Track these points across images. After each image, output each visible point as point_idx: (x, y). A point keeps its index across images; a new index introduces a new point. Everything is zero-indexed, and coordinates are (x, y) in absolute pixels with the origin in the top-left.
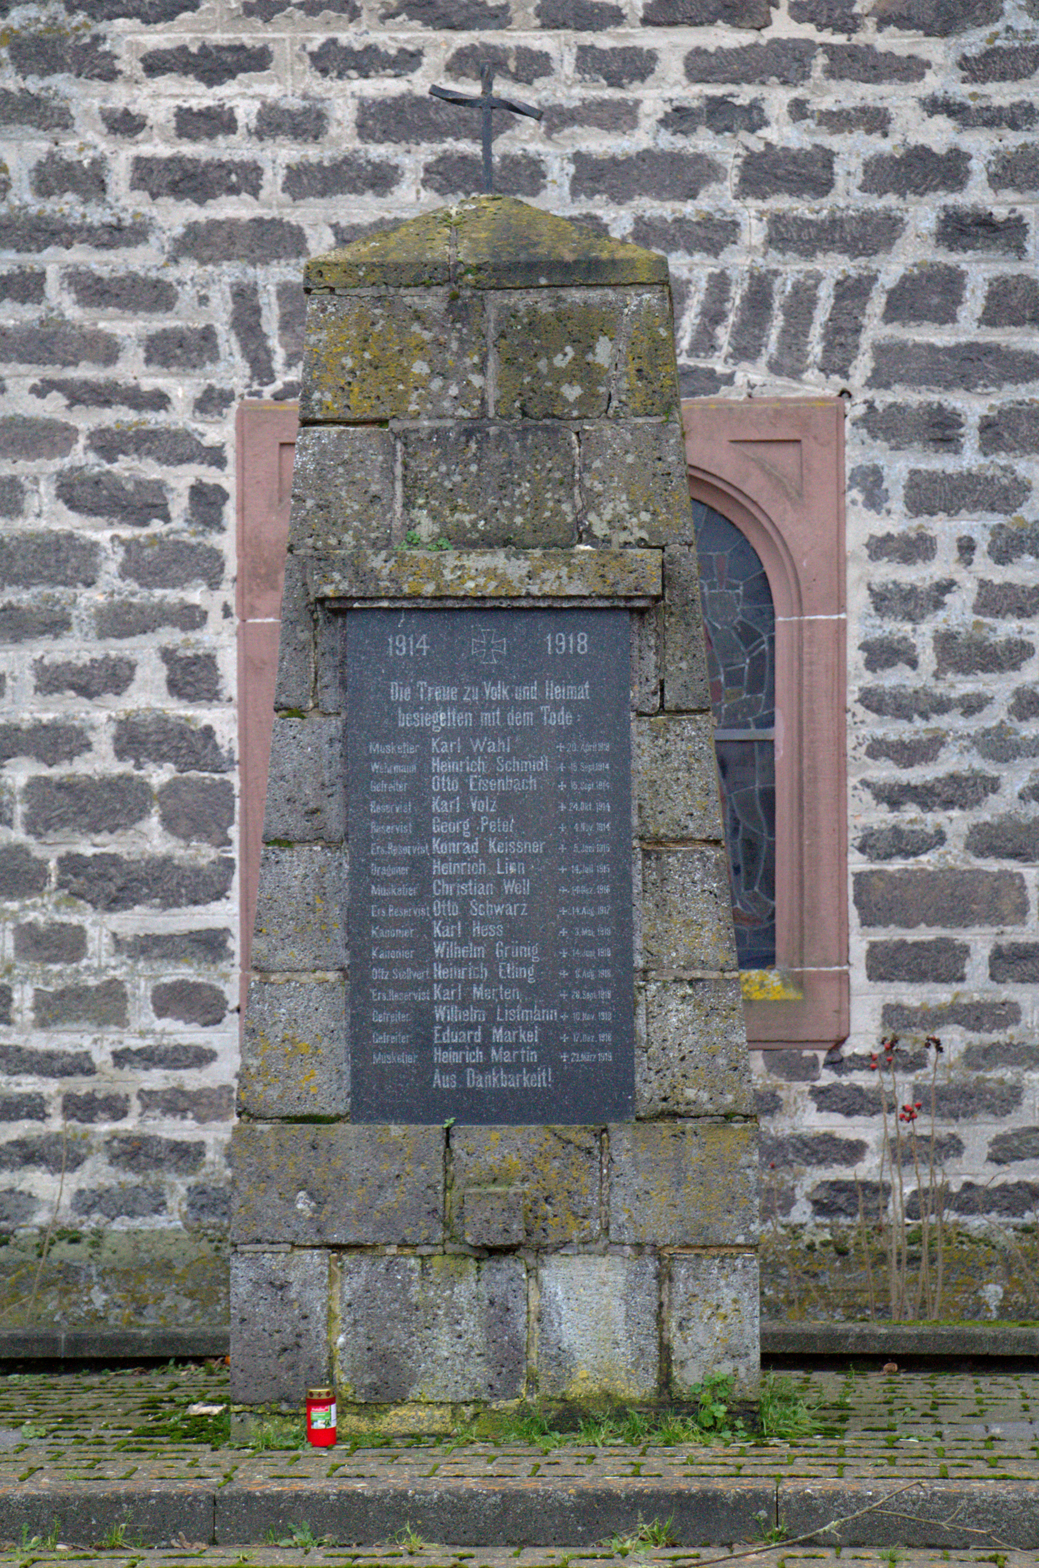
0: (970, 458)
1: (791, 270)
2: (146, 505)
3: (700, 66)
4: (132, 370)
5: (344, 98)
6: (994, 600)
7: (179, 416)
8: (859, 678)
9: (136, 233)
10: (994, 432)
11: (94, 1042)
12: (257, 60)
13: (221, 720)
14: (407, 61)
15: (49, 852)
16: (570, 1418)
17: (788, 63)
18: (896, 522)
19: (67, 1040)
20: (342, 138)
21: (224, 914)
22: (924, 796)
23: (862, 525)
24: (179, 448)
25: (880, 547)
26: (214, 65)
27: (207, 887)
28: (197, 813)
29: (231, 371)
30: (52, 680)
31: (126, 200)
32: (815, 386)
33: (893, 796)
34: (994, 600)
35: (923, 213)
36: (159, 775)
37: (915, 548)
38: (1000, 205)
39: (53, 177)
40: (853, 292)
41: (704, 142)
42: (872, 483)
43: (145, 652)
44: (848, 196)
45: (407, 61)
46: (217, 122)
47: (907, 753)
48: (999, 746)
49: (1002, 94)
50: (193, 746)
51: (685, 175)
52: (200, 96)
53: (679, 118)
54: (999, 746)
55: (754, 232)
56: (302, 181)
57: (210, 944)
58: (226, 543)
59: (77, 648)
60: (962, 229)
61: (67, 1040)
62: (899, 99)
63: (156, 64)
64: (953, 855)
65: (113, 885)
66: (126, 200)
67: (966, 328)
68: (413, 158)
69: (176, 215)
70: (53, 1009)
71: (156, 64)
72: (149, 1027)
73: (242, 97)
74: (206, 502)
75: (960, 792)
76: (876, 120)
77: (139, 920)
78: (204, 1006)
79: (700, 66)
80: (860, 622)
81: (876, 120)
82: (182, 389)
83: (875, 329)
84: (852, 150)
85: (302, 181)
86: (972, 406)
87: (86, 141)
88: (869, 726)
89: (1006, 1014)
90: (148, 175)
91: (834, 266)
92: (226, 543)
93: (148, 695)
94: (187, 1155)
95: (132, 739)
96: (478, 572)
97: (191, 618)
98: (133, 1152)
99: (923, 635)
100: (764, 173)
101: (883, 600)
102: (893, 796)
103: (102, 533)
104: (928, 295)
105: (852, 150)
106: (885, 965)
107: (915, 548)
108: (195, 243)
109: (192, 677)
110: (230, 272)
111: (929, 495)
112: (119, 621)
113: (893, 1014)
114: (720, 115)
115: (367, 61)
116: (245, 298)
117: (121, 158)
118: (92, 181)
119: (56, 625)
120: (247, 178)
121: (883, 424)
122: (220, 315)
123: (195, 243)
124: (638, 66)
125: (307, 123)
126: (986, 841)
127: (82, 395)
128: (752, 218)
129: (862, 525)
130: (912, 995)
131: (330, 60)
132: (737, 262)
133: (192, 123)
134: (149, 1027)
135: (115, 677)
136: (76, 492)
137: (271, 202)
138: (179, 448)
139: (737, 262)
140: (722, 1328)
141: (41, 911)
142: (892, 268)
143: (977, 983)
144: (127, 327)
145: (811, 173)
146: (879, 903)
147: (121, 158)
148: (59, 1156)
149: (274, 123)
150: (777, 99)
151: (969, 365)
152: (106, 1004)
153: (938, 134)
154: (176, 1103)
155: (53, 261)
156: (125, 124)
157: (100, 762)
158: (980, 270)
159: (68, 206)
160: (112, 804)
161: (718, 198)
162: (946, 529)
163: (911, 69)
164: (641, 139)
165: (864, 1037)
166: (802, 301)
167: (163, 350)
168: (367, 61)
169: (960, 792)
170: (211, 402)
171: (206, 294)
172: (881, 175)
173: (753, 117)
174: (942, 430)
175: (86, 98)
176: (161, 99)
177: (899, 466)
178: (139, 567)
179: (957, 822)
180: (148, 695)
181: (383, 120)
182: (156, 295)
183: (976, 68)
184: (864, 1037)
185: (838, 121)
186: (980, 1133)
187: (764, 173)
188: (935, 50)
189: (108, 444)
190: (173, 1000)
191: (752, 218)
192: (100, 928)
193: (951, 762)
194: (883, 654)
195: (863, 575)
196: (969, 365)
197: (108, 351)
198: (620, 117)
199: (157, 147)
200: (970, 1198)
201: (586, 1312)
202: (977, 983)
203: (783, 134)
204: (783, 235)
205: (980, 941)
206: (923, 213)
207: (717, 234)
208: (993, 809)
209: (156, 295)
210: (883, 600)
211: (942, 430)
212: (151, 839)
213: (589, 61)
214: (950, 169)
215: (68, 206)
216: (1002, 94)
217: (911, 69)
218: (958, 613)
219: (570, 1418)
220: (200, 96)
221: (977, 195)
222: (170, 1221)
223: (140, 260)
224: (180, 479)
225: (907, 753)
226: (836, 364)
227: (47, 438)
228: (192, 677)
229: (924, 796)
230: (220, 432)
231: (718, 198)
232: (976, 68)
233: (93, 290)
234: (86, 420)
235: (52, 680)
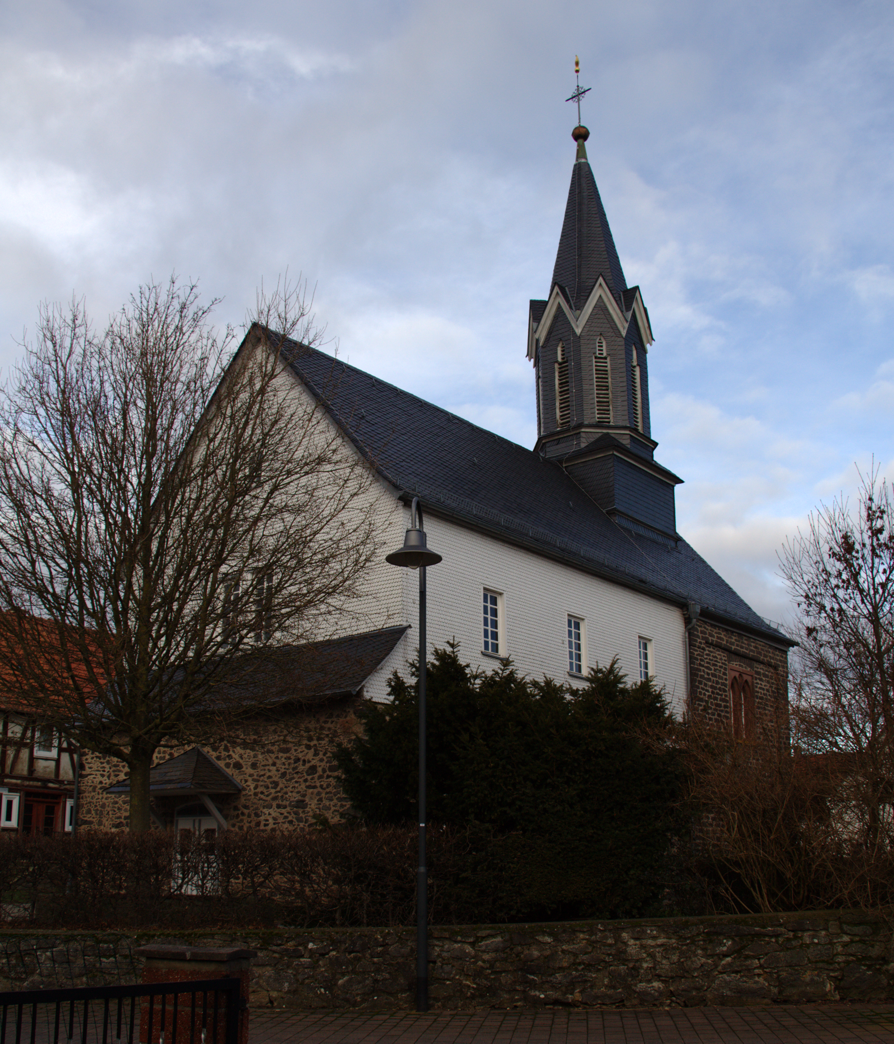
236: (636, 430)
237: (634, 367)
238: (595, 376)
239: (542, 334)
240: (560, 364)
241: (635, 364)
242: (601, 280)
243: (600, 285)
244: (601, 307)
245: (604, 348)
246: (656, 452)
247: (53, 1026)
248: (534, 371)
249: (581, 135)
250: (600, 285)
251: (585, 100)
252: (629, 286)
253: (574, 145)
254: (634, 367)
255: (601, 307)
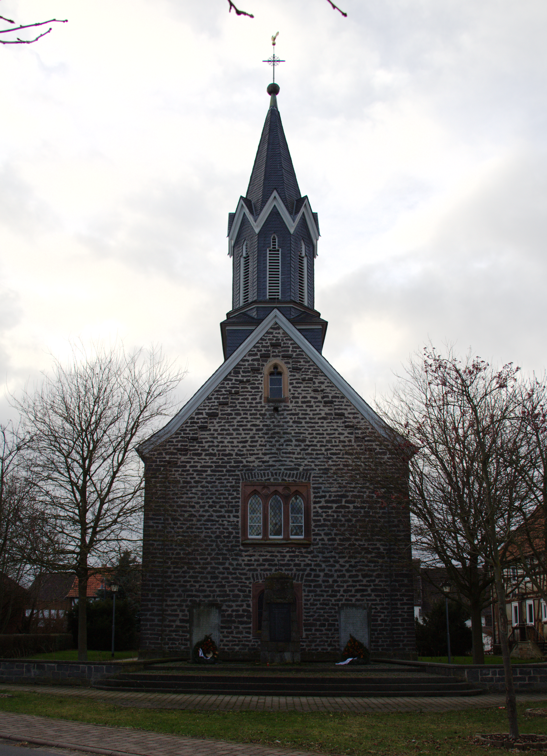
0: (312, 588)
1: (298, 573)
2: (245, 591)
3: (290, 556)
4: (244, 580)
5: (261, 559)
6: (314, 600)
7: (248, 584)
8: (304, 606)
9: (244, 569)
10: (314, 586)
11: (241, 636)
12: (254, 555)
13: (251, 609)
14: (266, 556)
15: (237, 620)
16: (287, 664)
17: (297, 556)
18: (306, 594)
19: (238, 636)
20: (261, 562)
21: (251, 625)
22: (309, 616)
23: (304, 594)
24: (248, 587)
25: (305, 596)
26: (251, 556)
27: (250, 623)
28: (249, 617)
29: (252, 581)
30: (237, 606)
31: (243, 566)
32: (300, 582)
33: (306, 616)
34: (314, 600)
35: (308, 568)
36: (246, 614)
37: (308, 596)
38: (315, 568)
39: (237, 565)
40: (303, 575)
41: (290, 562)
42: (304, 590)
43: (245, 603)
44: (302, 567)
45: (266, 556)
46: (251, 560)
47: (307, 613)
48: (315, 612)
49: (315, 559)
50: (248, 611)
51: (289, 565)
52: (249, 558)
53: (288, 560)
54: (315, 612)
55: (295, 570)
56: (258, 565)
57: (250, 628)
58: (251, 595)
59: (239, 603)
60: (312, 570)
61: (238, 636)
62: (306, 559)
63: (246, 556)
64: (311, 621)
65: (242, 623)
66: (243, 566)
67: (312, 578)
68: (267, 563)
69: (247, 568)
70: (237, 633)
71: (246, 556)
72: (245, 635)
73: (253, 558)
74: (250, 591)
75: (312, 616)
76: (304, 561)
77: (244, 626)
78: (249, 633)
79: (290, 556)
80: (303, 602)
81: (304, 561)
82: (248, 582)
83: (305, 578)
84: (303, 563)
85: (258, 565)
86: (313, 584)
87: (240, 562)
88: (304, 610)
89: (316, 634)
90: (245, 564)
91: (301, 573)
92: (251, 595)
93: (245, 607)
94: (248, 645)
95: (244, 611)
96: (279, 601)
97: (248, 601)
98: (243, 645)
99: (309, 603)
100: (295, 565)
101: (306, 600)
102: (306, 616)
103: (241, 594)
104: (309, 575)
105: (303, 563)
106: (306, 630)
107: (308, 596)
108: (249, 570)
109: (248, 606)
110: (252, 573)
111: (309, 591)
112: (242, 601)
113: (306, 634)
114: (292, 560)
115: (263, 556)
116: (253, 575)
117: (243, 563)
118: (241, 565)
119: (237, 601)
120: (253, 565)
121: (305, 585)
122: (251, 576)
123: (249, 570)
124: (285, 556)
125: (258, 560)
126: (314, 620)
127: (239, 582)
128: (294, 569)
129: (304, 594)
130: (308, 633)
131: (260, 555)
132: (293, 572)
133: (249, 560)
134: (245, 635)
135: (242, 605)
136: (239, 590)
137: (255, 567)
138: (248, 587)
139: (293, 572)
140: (298, 657)
141: (236, 625)
142: (306, 573)
143: (313, 632)
144: (243, 577)
145: (299, 565)
146: (305, 625)
147: (243, 563)
148: (238, 645)
149: (255, 560)
150: (296, 559)
151: (312, 581)
152: (241, 633)
153: (309, 562)
154: (247, 641)
155: (237, 571)
156: (243, 560)
157: (241, 613)
158: (313, 573)
159: (239, 567)
160: (242, 616)
161: (292, 567)
162: (310, 594)
163: (307, 557)
164: (285, 562)
165: (304, 636)
166: (299, 575)
167: (246, 579)
168: (263, 556)
169: (312, 616)
170: (250, 583)
171: (250, 574)
172: (305, 565)
173: (295, 560)
174: (310, 586)
175: (240, 558)
176: (246, 559)
177: (307, 589)
178: (244, 596)
179: (312, 618)
180: (245, 607)
181: (264, 560)
182: (246, 574)
183: (312, 557)
184: (304, 636)
185: (301, 561)
186: (313, 644)
187: (295, 565)
188: (309, 555)
189: (242, 586)
190: (247, 632)
191: (294, 569)
192: (241, 626)
193: (311, 613)
194: (305, 604)
195: (304, 598)
196: (312, 581)
197: (242, 579)
198: (284, 560)
199: (246, 562)
200: (313, 650)
201: (287, 656)
202: (313, 632)
203: (297, 562)
204: (297, 570)
205: (313, 628)
206: (308, 568)
207: (292, 570)
208: (314, 617)
209: (246, 574)
210: (306, 600)
211: (310, 586)
212: (245, 619)
213: (281, 556)
214: (310, 565)
215: (239, 567)
216: (315, 559)
217: (307, 557)
218: (312, 601)
219: (287, 664)
220: (249, 558)
221: (313, 567)
222: (247, 651)
223: (244, 571)
224: (248, 589)
225: (307, 613)
226: (302, 580)
227: (237, 586)
228: (248, 606)
229: (309, 616)
230: (251, 586)
231: (292, 567)
232: (312, 557)
233: (240, 574)
234: (240, 584)
235: (237, 606)
236: (302, 305)
237: (303, 257)
238: (240, 508)
239: (233, 242)
240: (245, 258)
241: (303, 255)
242: (275, 193)
243: (275, 197)
244: (275, 213)
245: (277, 244)
246: (321, 317)
247: (97, 472)
248: (230, 261)
249: (273, 90)
250: (275, 197)
251: (269, 57)
252: (302, 196)
253: (269, 97)
254: (303, 257)
255: (275, 213)
